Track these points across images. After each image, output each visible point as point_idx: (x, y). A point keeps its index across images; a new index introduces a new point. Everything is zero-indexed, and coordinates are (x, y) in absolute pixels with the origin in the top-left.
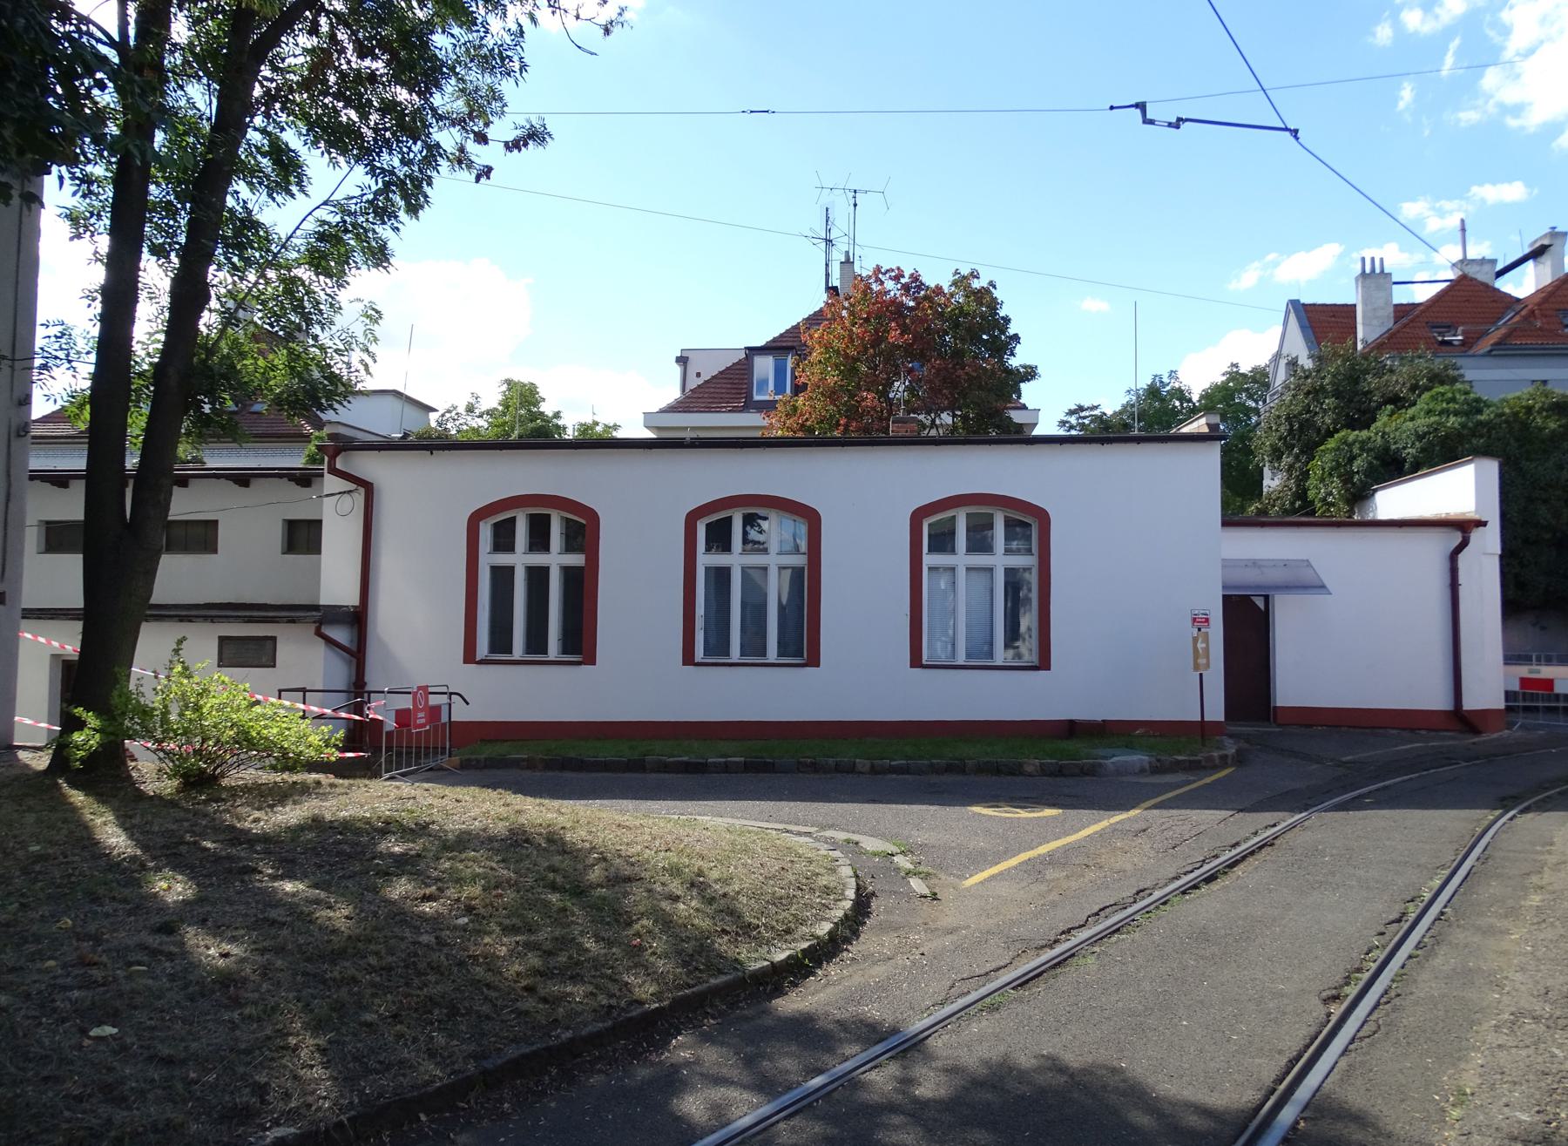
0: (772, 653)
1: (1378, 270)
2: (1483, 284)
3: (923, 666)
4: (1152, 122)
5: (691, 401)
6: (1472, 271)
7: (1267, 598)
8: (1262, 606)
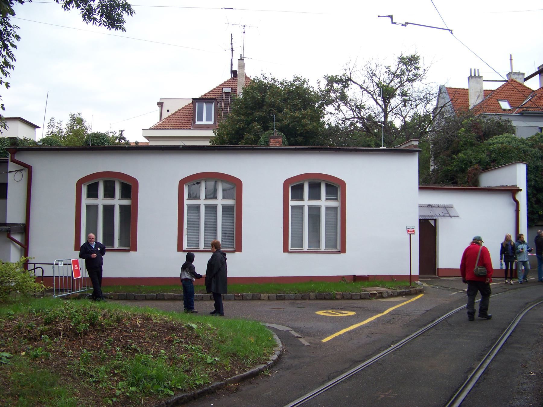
0: (306, 248)
1: (477, 75)
2: (520, 84)
3: (288, 251)
4: (395, 23)
5: (164, 124)
6: (513, 77)
7: (435, 220)
8: (433, 225)
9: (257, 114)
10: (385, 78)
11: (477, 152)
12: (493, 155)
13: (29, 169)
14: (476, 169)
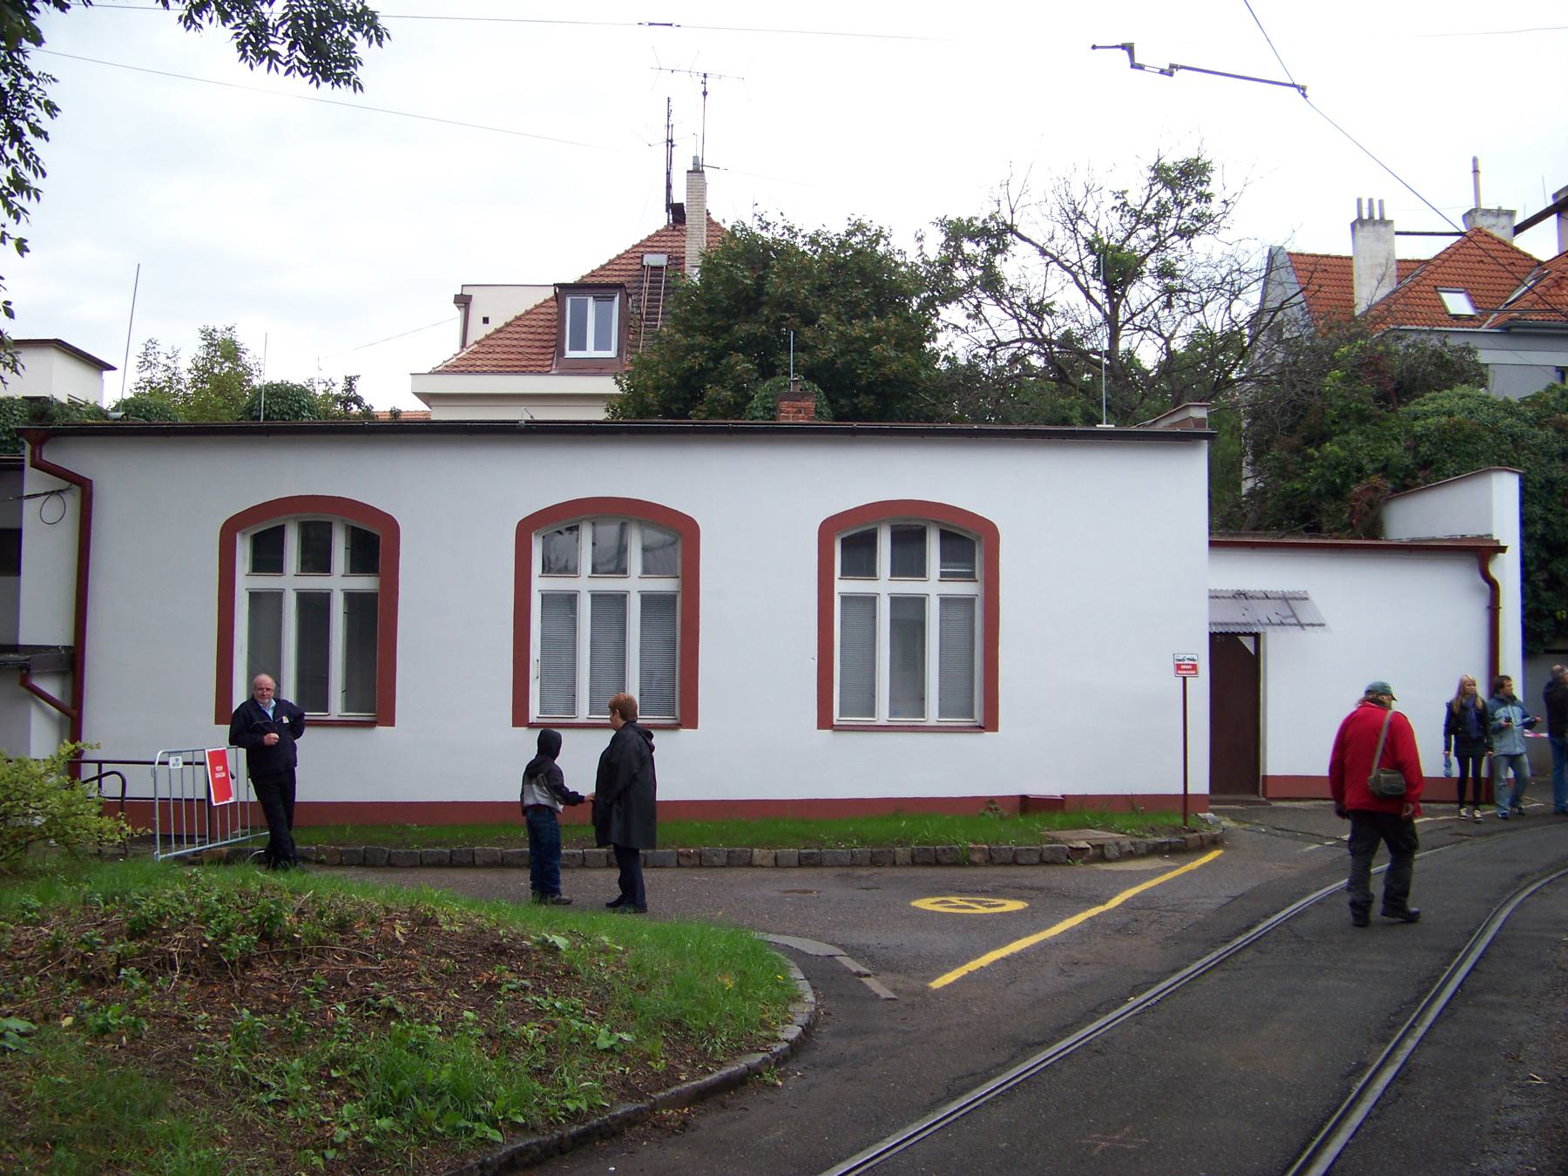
0: (883, 715)
1: (1377, 217)
2: (1500, 242)
3: (831, 726)
4: (1141, 67)
5: (475, 357)
6: (1483, 222)
7: (1257, 636)
8: (1251, 649)
9: (742, 329)
10: (1111, 227)
11: (1377, 439)
12: (1424, 449)
13: (84, 488)
14: (1376, 489)
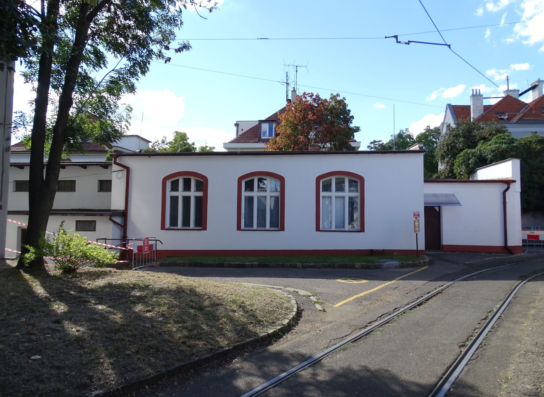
0: (268, 226)
1: (478, 94)
2: (514, 98)
3: (320, 231)
4: (400, 42)
5: (240, 139)
6: (511, 94)
7: (439, 207)
8: (438, 210)
